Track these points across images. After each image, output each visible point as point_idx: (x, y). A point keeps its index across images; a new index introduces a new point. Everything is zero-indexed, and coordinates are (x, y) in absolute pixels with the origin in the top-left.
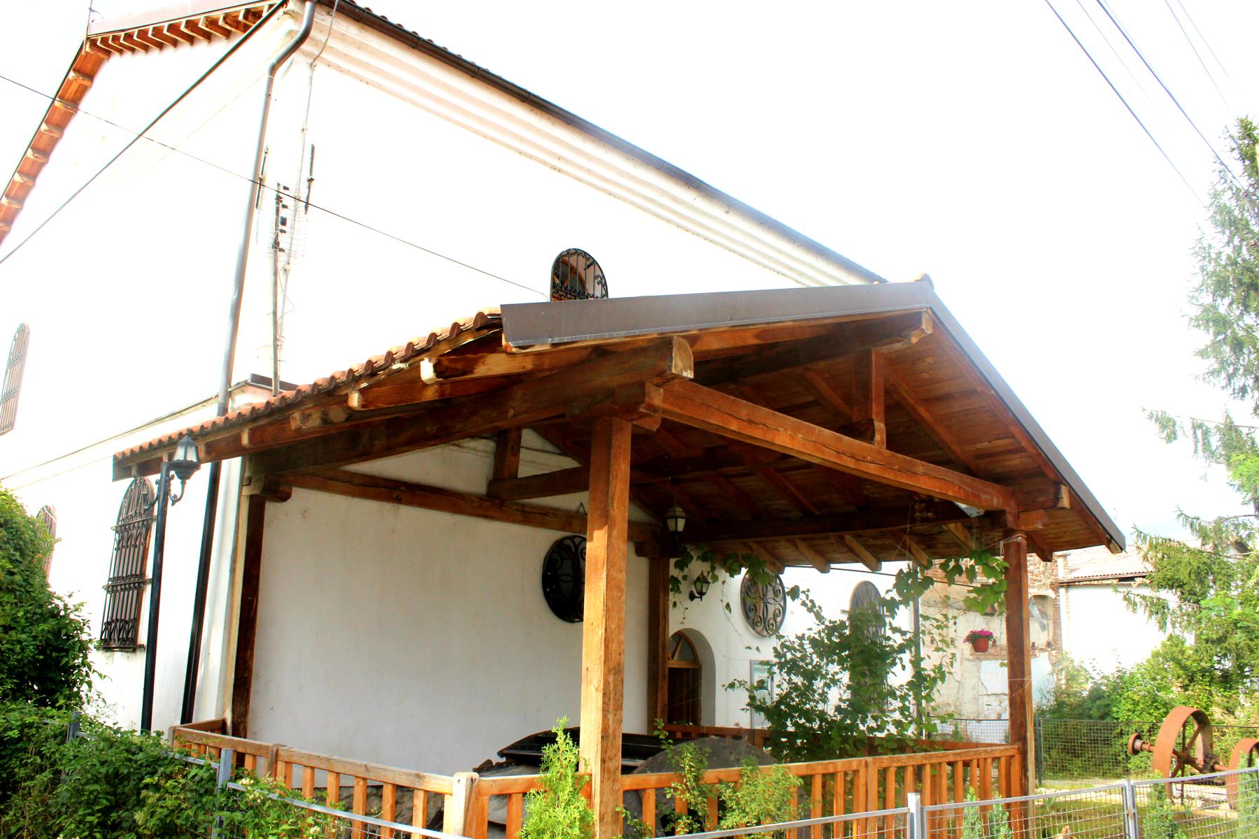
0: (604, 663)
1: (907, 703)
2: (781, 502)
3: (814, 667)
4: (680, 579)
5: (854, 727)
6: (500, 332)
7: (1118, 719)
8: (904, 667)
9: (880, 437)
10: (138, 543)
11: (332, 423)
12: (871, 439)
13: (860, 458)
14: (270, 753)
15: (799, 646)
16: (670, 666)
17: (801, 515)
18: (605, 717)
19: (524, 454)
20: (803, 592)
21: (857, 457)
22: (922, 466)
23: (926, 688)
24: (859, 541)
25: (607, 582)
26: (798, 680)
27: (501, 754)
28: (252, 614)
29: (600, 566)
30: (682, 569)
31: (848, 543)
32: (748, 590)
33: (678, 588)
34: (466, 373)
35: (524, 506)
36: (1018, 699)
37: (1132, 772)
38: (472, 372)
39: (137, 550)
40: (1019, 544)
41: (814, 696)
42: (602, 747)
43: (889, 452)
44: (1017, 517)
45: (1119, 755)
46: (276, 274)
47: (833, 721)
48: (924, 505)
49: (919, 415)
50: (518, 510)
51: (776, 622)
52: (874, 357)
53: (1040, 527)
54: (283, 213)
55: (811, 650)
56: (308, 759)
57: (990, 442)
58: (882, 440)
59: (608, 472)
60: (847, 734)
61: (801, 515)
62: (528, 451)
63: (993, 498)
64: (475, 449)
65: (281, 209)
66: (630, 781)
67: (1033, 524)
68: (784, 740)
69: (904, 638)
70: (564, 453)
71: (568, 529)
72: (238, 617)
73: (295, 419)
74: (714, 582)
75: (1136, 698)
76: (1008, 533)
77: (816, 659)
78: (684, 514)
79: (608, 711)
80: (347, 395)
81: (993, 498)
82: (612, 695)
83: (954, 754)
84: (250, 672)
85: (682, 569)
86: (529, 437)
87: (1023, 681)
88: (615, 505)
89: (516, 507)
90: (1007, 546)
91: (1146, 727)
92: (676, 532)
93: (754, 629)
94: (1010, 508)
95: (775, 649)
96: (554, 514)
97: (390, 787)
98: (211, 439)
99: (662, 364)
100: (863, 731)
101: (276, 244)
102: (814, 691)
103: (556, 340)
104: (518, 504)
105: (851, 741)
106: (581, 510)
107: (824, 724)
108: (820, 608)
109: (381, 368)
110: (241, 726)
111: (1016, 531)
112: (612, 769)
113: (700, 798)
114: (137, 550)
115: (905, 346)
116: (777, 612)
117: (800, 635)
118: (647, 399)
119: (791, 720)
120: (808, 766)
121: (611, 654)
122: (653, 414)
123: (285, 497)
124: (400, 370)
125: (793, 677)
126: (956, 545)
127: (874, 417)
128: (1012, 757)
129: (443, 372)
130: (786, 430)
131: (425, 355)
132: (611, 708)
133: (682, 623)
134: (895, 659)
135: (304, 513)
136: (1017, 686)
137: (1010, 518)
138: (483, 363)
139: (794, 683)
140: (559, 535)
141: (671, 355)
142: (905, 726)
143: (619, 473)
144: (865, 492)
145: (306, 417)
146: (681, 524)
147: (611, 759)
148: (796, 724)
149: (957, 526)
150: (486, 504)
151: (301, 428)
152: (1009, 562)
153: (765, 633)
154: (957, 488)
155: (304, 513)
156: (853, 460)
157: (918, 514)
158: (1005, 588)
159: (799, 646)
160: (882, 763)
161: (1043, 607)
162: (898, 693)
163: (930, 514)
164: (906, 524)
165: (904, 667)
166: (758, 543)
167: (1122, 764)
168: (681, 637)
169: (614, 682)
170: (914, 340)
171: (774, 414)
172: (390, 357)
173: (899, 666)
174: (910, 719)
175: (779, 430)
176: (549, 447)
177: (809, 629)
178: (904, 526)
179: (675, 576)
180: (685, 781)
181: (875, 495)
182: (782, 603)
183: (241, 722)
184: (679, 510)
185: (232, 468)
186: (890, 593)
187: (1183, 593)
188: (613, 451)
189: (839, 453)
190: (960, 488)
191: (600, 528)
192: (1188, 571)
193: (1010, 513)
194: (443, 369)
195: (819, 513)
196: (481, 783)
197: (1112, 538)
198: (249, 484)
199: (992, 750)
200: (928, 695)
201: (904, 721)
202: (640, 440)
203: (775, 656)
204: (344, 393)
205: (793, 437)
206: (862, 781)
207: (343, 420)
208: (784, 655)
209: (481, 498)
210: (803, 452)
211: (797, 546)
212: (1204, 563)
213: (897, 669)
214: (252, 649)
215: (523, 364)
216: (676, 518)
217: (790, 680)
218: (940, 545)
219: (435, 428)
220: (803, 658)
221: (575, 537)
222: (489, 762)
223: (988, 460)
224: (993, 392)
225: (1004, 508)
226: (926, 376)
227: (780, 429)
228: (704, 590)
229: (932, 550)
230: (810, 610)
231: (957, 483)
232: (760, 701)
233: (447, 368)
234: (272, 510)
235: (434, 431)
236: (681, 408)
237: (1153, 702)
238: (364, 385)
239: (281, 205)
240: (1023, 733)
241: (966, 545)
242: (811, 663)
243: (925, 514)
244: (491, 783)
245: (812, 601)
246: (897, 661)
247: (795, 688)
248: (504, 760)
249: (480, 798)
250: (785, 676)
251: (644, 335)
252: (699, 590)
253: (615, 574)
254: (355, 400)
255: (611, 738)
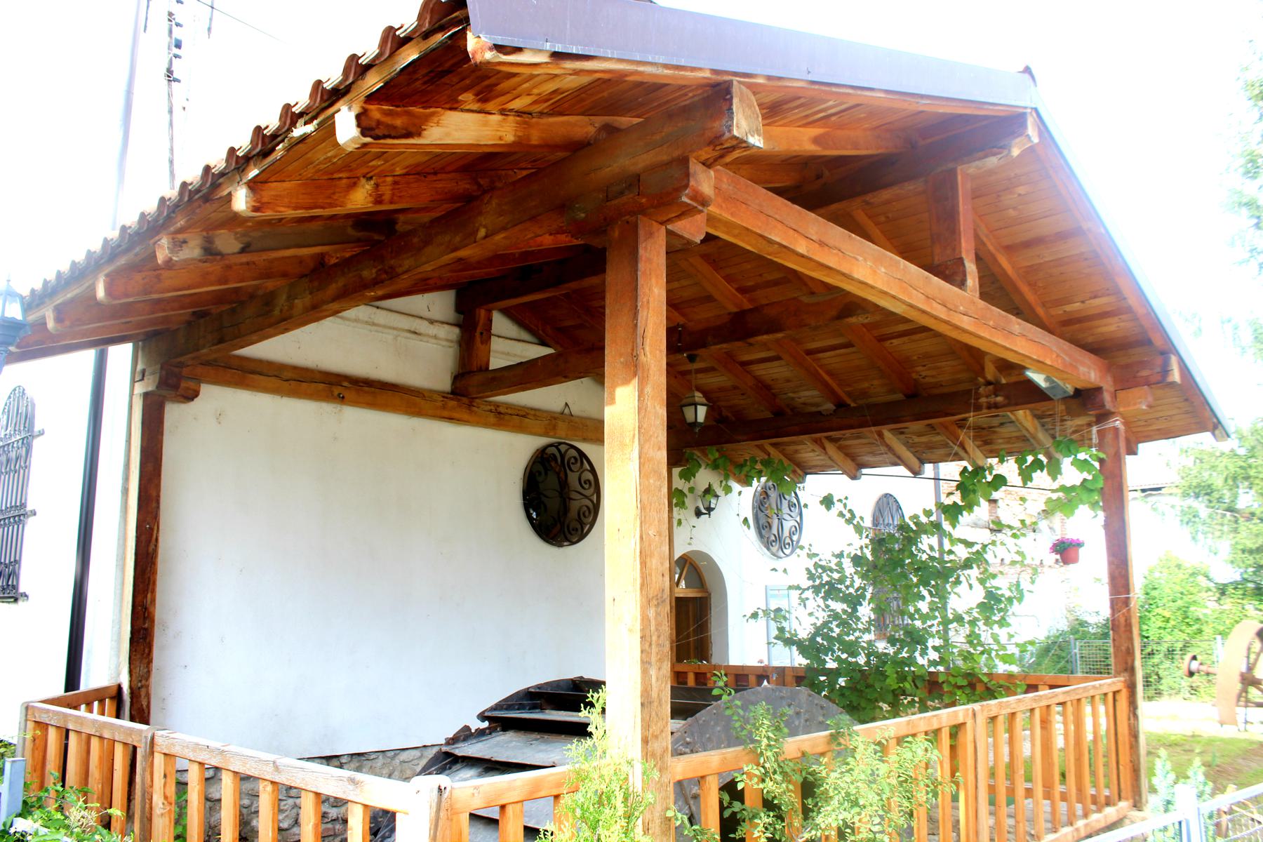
0: (641, 589)
1: (976, 630)
2: (807, 393)
3: (857, 590)
4: (686, 491)
5: (911, 661)
6: (463, 32)
7: (1147, 637)
8: (971, 586)
9: (972, 281)
10: (17, 467)
11: (220, 254)
12: (962, 284)
13: (952, 307)
14: (144, 740)
15: (836, 565)
16: (677, 595)
17: (834, 408)
18: (645, 672)
19: (496, 344)
20: (840, 501)
21: (948, 305)
22: (1019, 324)
23: (1000, 610)
24: (898, 439)
25: (641, 465)
26: (838, 606)
27: (482, 717)
28: (152, 547)
29: (627, 441)
30: (688, 480)
31: (888, 441)
32: (761, 503)
33: (683, 503)
34: (408, 135)
35: (497, 405)
36: (1122, 620)
37: (1165, 693)
38: (419, 134)
39: (16, 475)
40: (1116, 429)
41: (857, 624)
42: (643, 720)
43: (982, 304)
44: (1115, 397)
45: (1150, 677)
46: (171, 112)
47: (886, 654)
48: (991, 387)
49: (1000, 266)
50: (491, 411)
51: (792, 541)
52: (959, 178)
53: (1144, 407)
54: (177, 33)
55: (852, 570)
56: (194, 751)
57: (1083, 302)
58: (974, 285)
59: (635, 298)
60: (910, 669)
61: (834, 408)
62: (501, 340)
63: (1089, 372)
64: (435, 337)
65: (174, 26)
66: (683, 767)
67: (1135, 404)
68: (822, 678)
69: (970, 550)
70: (543, 343)
71: (551, 434)
72: (133, 551)
73: (162, 247)
74: (726, 494)
75: (1167, 614)
76: (1103, 416)
77: (858, 582)
78: (704, 401)
79: (650, 663)
80: (230, 194)
81: (1089, 372)
82: (654, 638)
83: (1064, 693)
84: (153, 621)
85: (688, 480)
86: (500, 323)
87: (1128, 598)
88: (647, 348)
89: (489, 408)
90: (1101, 434)
91: (1179, 645)
92: (695, 423)
93: (768, 549)
94: (1107, 385)
95: (808, 569)
96: (535, 415)
97: (311, 796)
98: (59, 300)
99: (716, 124)
100: (923, 665)
101: (170, 72)
102: (858, 619)
103: (559, 48)
104: (490, 403)
105: (909, 678)
106: (567, 411)
107: (872, 658)
108: (862, 518)
109: (276, 137)
110: (143, 692)
111: (1113, 413)
112: (659, 752)
113: (784, 785)
114: (16, 475)
115: (1002, 162)
116: (793, 529)
117: (837, 552)
118: (692, 183)
119: (832, 655)
120: (908, 723)
121: (651, 575)
122: (700, 208)
123: (191, 396)
124: (304, 139)
125: (830, 602)
126: (1024, 439)
127: (964, 256)
128: (1118, 691)
129: (372, 129)
130: (865, 260)
131: (341, 102)
132: (654, 659)
133: (690, 544)
134: (959, 576)
135: (219, 417)
136: (1120, 605)
137: (1107, 397)
138: (438, 123)
139: (832, 610)
140: (541, 441)
141: (730, 109)
142: (975, 657)
143: (651, 300)
144: (914, 376)
145: (178, 244)
146: (702, 412)
147: (656, 737)
148: (838, 659)
149: (1025, 412)
150: (452, 403)
151: (171, 259)
152: (1104, 452)
153: (781, 554)
154: (1054, 356)
155: (219, 417)
156: (945, 309)
157: (983, 400)
158: (1100, 484)
159: (836, 565)
160: (991, 710)
161: (1051, 522)
162: (967, 618)
163: (999, 399)
164: (970, 412)
165: (971, 586)
166: (774, 445)
167: (1154, 687)
168: (686, 561)
169: (656, 618)
170: (1015, 152)
171: (850, 236)
172: (290, 117)
173: (964, 585)
174: (980, 649)
175: (857, 260)
176: (525, 335)
177: (849, 545)
178: (967, 415)
179: (680, 488)
180: (762, 761)
181: (927, 380)
182: (798, 519)
183: (142, 686)
184: (698, 396)
185: (121, 356)
186: (951, 497)
187: (1210, 501)
188: (641, 266)
189: (927, 297)
190: (1058, 356)
191: (626, 382)
192: (1224, 476)
193: (1107, 391)
194: (373, 124)
195: (855, 405)
196: (456, 793)
197: (1219, 422)
198: (142, 379)
199: (1100, 685)
200: (1003, 618)
201: (973, 651)
202: (677, 252)
203: (809, 579)
204: (225, 193)
205: (875, 272)
206: (969, 737)
207: (236, 250)
208: (820, 577)
209: (444, 395)
210: (885, 293)
211: (824, 449)
212: (1241, 467)
213: (962, 588)
214: (153, 591)
215: (499, 134)
216: (695, 405)
217: (827, 606)
218: (1000, 441)
219: (374, 271)
220: (841, 581)
221: (560, 443)
222: (467, 728)
223: (1077, 326)
224: (1102, 230)
225: (1102, 385)
226: (1012, 213)
227: (858, 257)
228: (712, 506)
229: (988, 447)
230: (849, 521)
231: (1054, 349)
232: (790, 632)
233: (379, 123)
234: (174, 413)
235: (374, 276)
236: (732, 214)
237: (1184, 618)
238: (253, 173)
239: (173, 23)
240: (1130, 662)
241: (1034, 438)
242: (852, 585)
243: (992, 399)
244: (472, 791)
245: (850, 511)
246: (962, 578)
247: (835, 616)
248: (486, 724)
249: (455, 818)
250: (821, 602)
251: (693, 69)
252: (706, 505)
253: (651, 453)
254: (241, 200)
255: (656, 704)
